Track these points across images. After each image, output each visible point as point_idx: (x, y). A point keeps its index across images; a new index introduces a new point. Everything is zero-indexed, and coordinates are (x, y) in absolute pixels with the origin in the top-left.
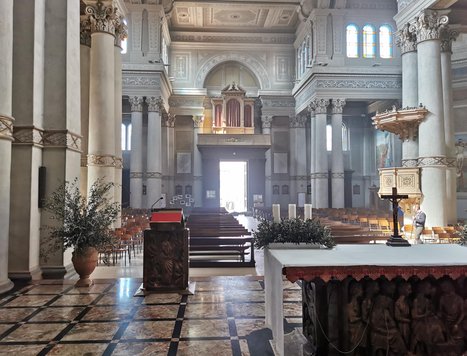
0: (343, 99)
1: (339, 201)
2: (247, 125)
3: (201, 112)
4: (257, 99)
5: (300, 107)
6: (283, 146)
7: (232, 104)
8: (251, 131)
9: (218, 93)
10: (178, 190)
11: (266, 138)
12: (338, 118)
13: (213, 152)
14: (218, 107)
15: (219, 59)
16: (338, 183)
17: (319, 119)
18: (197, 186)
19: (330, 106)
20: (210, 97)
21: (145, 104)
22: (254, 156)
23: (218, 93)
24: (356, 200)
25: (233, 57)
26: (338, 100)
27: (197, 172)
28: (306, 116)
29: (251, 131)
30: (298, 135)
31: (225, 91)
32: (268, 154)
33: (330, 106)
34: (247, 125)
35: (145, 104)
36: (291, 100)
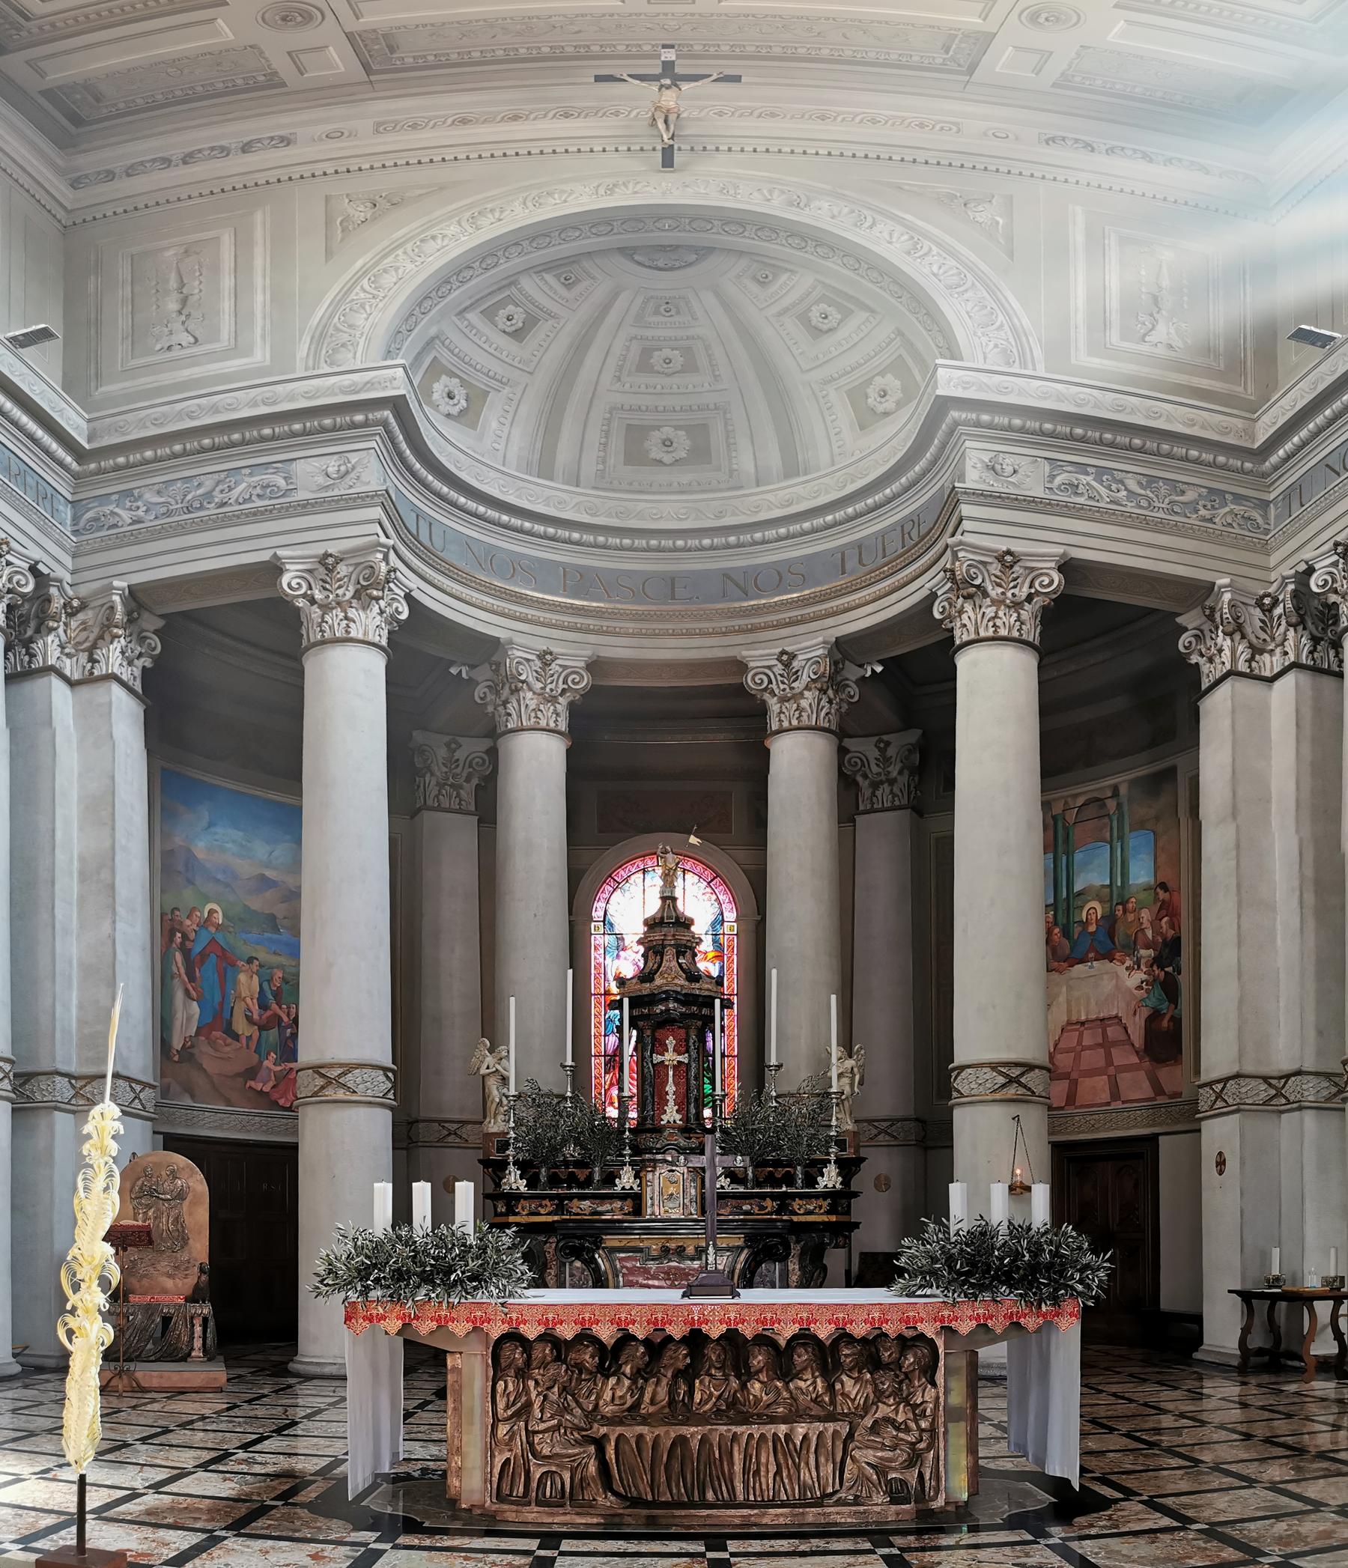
0: (811, 647)
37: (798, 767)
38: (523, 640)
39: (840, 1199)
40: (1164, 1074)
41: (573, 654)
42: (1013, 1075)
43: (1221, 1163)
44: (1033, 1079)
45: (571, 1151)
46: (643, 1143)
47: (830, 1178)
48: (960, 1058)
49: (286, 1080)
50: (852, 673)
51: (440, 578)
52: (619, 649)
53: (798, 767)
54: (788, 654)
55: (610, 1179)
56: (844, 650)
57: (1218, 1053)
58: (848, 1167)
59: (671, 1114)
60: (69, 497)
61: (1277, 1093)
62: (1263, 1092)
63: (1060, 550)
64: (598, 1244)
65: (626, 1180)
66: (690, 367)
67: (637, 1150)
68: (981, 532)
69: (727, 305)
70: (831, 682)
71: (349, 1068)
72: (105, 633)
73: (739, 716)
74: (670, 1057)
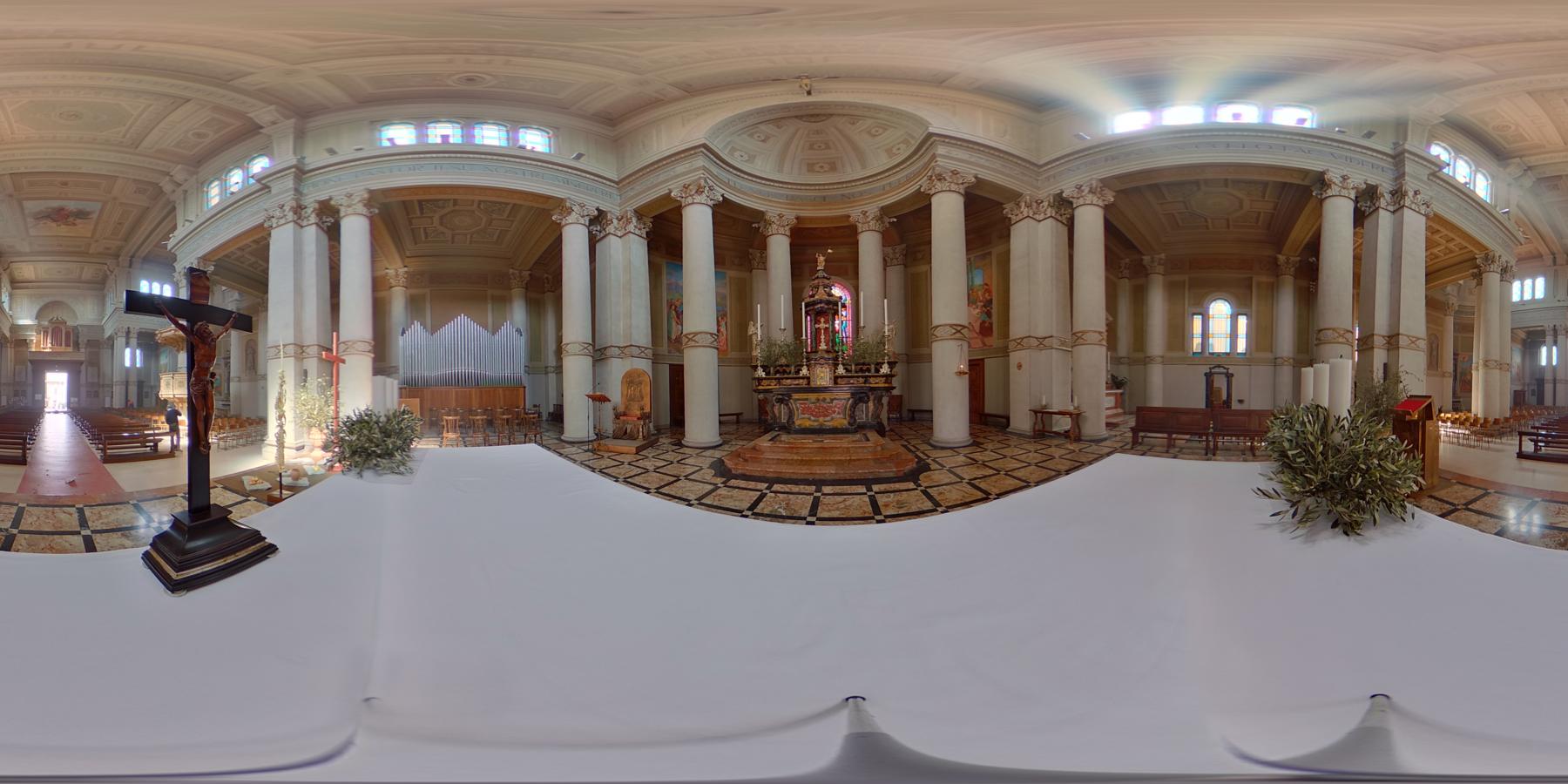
0: (873, 209)
1: (133, 399)
2: (67, 345)
3: (33, 337)
4: (75, 328)
5: (108, 333)
6: (94, 362)
7: (56, 331)
8: (70, 349)
9: (46, 323)
10: (16, 394)
11: (82, 356)
12: (134, 341)
13: (42, 364)
14: (46, 333)
15: (47, 300)
16: (133, 389)
17: (120, 341)
18: (29, 390)
19: (128, 333)
20: (39, 325)
21: (1555, 330)
22: (73, 368)
23: (46, 323)
24: (146, 402)
25: (58, 299)
26: (864, 213)
27: (30, 381)
28: (111, 339)
29: (70, 349)
30: (105, 354)
31: (51, 321)
32: (83, 367)
33: (128, 333)
34: (67, 345)
35: (1555, 330)
36: (102, 329)
37: (869, 246)
38: (772, 211)
39: (888, 377)
40: (987, 340)
41: (790, 215)
42: (958, 329)
43: (1020, 366)
44: (965, 331)
45: (783, 361)
46: (811, 359)
47: (885, 369)
48: (935, 322)
49: (678, 340)
50: (887, 220)
51: (739, 181)
52: (803, 214)
53: (869, 246)
54: (865, 213)
55: (798, 372)
56: (885, 211)
57: (1017, 330)
58: (892, 365)
59: (823, 346)
60: (614, 176)
61: (1042, 343)
62: (1035, 342)
63: (974, 170)
64: (790, 397)
65: (804, 371)
66: (828, 147)
67: (809, 359)
68: (946, 158)
69: (841, 132)
70: (880, 219)
71: (696, 334)
72: (629, 222)
73: (846, 234)
74: (822, 325)
